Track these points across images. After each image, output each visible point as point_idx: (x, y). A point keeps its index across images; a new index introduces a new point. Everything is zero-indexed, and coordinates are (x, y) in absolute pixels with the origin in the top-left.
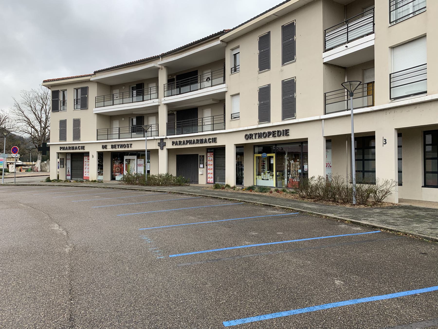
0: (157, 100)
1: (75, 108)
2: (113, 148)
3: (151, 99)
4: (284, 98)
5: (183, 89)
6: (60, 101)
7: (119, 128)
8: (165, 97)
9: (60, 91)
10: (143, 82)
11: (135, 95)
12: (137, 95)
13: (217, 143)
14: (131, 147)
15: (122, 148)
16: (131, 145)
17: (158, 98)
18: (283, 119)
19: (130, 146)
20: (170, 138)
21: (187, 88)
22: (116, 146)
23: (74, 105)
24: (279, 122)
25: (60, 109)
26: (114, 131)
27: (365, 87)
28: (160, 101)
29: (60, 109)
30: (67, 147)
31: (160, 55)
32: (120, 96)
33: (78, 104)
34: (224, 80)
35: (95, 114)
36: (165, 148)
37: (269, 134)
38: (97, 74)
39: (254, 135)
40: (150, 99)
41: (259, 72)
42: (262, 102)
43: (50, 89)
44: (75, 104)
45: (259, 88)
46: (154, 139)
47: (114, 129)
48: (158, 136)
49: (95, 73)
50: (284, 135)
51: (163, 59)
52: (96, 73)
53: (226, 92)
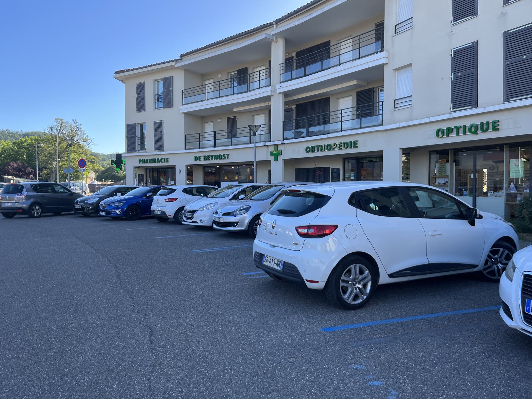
0: (269, 88)
1: (156, 107)
2: (197, 161)
3: (260, 87)
4: (507, 62)
5: (309, 68)
6: (137, 138)
7: (215, 132)
8: (281, 82)
9: (137, 125)
10: (247, 67)
11: (235, 84)
12: (239, 84)
13: (499, 131)
14: (228, 158)
15: (217, 159)
16: (228, 155)
17: (270, 85)
18: (508, 98)
19: (226, 156)
20: (288, 144)
21: (317, 66)
22: (210, 158)
23: (155, 102)
24: (500, 104)
25: (137, 149)
26: (207, 136)
27: (377, 109)
28: (273, 90)
29: (137, 149)
30: (147, 160)
31: (274, 21)
32: (216, 89)
33: (160, 101)
34: (382, 47)
35: (182, 113)
36: (281, 158)
37: (450, 131)
38: (184, 58)
39: (316, 148)
40: (259, 88)
41: (453, 23)
42: (460, 74)
43: (124, 83)
44: (156, 101)
45: (453, 50)
46: (265, 146)
47: (207, 134)
48: (271, 140)
49: (181, 58)
50: (353, 147)
51: (279, 26)
52: (182, 56)
53: (386, 65)
